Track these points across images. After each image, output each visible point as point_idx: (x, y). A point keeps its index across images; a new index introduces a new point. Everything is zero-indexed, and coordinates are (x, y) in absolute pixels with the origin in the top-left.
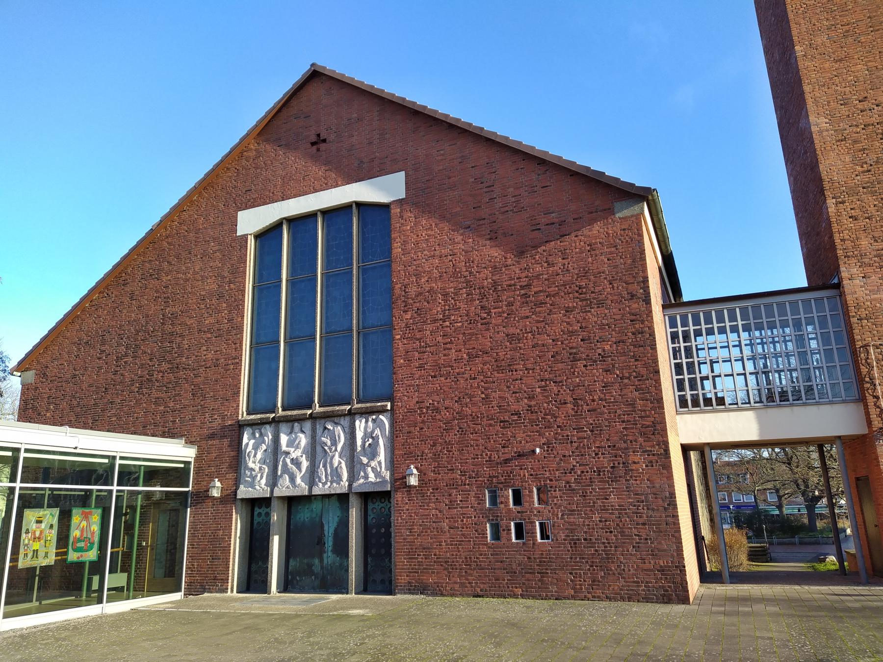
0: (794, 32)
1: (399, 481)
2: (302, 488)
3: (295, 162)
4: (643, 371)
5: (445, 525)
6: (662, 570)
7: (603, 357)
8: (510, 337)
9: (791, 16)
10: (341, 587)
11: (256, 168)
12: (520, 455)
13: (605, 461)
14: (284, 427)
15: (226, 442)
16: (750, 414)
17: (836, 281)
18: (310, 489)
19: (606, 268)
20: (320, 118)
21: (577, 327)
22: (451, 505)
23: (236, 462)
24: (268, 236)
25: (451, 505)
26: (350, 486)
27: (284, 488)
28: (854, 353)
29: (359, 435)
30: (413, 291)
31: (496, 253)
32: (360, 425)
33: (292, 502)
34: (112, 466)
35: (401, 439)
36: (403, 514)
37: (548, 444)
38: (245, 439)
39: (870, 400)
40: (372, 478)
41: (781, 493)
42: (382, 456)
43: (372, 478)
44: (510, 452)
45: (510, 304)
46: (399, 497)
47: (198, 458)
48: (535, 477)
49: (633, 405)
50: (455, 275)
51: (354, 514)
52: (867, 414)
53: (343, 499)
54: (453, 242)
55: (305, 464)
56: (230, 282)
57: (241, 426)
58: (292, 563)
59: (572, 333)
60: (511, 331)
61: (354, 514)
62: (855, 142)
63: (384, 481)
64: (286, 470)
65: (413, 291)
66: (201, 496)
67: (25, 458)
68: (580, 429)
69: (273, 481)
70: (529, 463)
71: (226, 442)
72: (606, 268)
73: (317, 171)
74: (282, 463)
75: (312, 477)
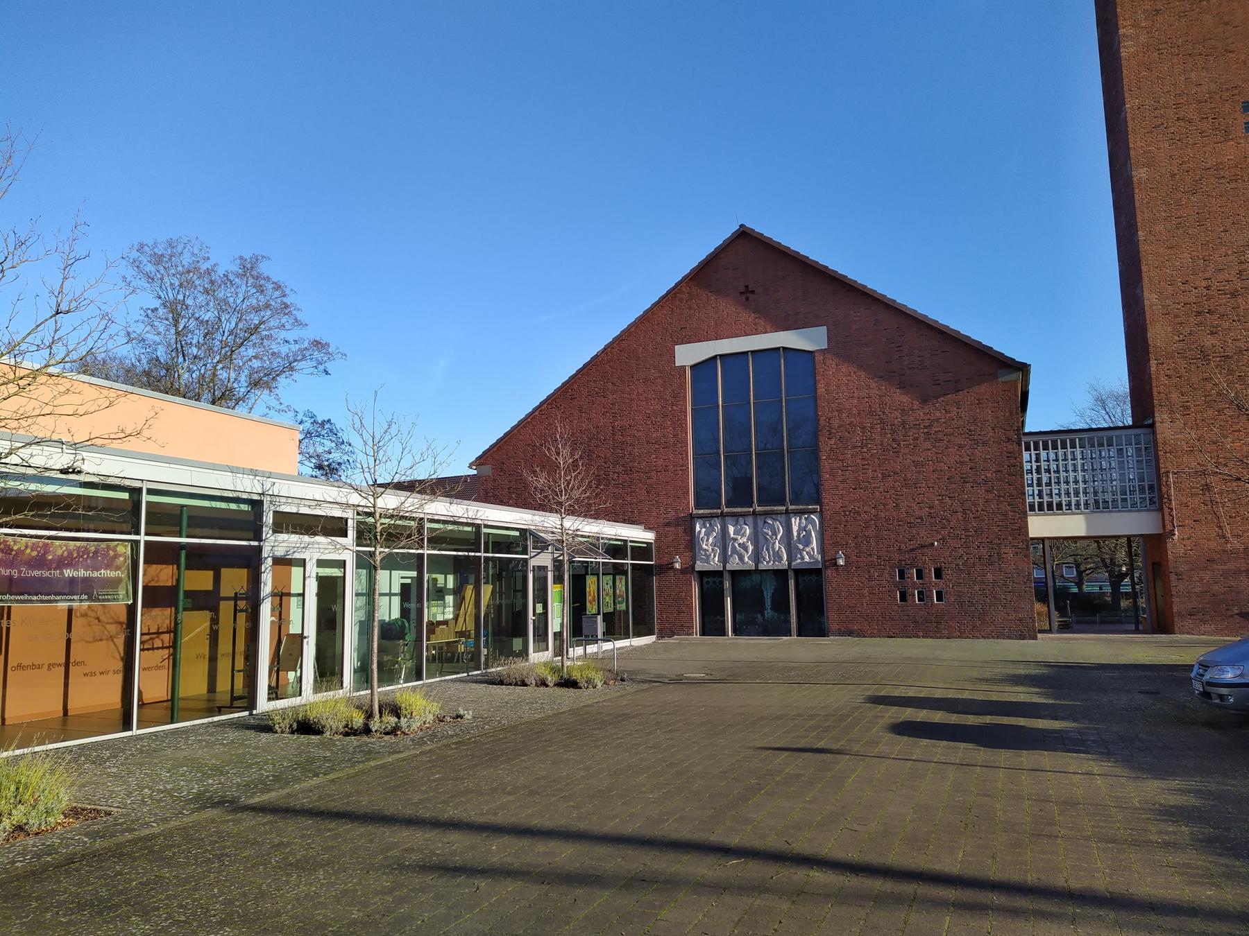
0: (1139, 218)
1: (831, 563)
2: (749, 564)
3: (726, 307)
4: (1014, 493)
5: (866, 592)
6: (1020, 620)
7: (986, 482)
8: (916, 464)
9: (1137, 204)
10: (788, 633)
11: (690, 309)
12: (922, 546)
13: (984, 552)
14: (728, 519)
15: (681, 529)
16: (1081, 517)
17: (1150, 421)
18: (757, 565)
19: (990, 418)
20: (749, 272)
21: (967, 459)
22: (870, 579)
23: (692, 544)
24: (703, 368)
25: (870, 579)
26: (790, 564)
27: (734, 564)
28: (1159, 476)
29: (795, 528)
30: (836, 423)
31: (905, 399)
32: (795, 523)
33: (734, 573)
34: (136, 505)
35: (829, 532)
36: (833, 584)
37: (943, 539)
38: (698, 528)
39: (1166, 511)
40: (807, 558)
41: (1082, 568)
42: (814, 544)
43: (807, 558)
44: (914, 544)
45: (915, 439)
46: (829, 573)
47: (656, 540)
48: (933, 561)
49: (1006, 515)
50: (871, 413)
51: (792, 583)
52: (1163, 520)
53: (781, 575)
54: (869, 387)
55: (751, 548)
56: (672, 405)
57: (692, 518)
58: (738, 616)
59: (963, 463)
60: (917, 459)
61: (792, 583)
62: (1176, 316)
63: (817, 561)
64: (734, 551)
65: (836, 423)
66: (666, 568)
67: (147, 502)
68: (966, 530)
69: (724, 559)
70: (929, 552)
71: (681, 529)
72: (990, 418)
73: (747, 317)
74: (727, 544)
75: (757, 557)
